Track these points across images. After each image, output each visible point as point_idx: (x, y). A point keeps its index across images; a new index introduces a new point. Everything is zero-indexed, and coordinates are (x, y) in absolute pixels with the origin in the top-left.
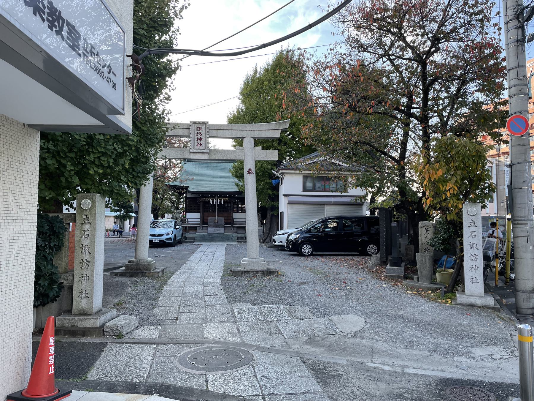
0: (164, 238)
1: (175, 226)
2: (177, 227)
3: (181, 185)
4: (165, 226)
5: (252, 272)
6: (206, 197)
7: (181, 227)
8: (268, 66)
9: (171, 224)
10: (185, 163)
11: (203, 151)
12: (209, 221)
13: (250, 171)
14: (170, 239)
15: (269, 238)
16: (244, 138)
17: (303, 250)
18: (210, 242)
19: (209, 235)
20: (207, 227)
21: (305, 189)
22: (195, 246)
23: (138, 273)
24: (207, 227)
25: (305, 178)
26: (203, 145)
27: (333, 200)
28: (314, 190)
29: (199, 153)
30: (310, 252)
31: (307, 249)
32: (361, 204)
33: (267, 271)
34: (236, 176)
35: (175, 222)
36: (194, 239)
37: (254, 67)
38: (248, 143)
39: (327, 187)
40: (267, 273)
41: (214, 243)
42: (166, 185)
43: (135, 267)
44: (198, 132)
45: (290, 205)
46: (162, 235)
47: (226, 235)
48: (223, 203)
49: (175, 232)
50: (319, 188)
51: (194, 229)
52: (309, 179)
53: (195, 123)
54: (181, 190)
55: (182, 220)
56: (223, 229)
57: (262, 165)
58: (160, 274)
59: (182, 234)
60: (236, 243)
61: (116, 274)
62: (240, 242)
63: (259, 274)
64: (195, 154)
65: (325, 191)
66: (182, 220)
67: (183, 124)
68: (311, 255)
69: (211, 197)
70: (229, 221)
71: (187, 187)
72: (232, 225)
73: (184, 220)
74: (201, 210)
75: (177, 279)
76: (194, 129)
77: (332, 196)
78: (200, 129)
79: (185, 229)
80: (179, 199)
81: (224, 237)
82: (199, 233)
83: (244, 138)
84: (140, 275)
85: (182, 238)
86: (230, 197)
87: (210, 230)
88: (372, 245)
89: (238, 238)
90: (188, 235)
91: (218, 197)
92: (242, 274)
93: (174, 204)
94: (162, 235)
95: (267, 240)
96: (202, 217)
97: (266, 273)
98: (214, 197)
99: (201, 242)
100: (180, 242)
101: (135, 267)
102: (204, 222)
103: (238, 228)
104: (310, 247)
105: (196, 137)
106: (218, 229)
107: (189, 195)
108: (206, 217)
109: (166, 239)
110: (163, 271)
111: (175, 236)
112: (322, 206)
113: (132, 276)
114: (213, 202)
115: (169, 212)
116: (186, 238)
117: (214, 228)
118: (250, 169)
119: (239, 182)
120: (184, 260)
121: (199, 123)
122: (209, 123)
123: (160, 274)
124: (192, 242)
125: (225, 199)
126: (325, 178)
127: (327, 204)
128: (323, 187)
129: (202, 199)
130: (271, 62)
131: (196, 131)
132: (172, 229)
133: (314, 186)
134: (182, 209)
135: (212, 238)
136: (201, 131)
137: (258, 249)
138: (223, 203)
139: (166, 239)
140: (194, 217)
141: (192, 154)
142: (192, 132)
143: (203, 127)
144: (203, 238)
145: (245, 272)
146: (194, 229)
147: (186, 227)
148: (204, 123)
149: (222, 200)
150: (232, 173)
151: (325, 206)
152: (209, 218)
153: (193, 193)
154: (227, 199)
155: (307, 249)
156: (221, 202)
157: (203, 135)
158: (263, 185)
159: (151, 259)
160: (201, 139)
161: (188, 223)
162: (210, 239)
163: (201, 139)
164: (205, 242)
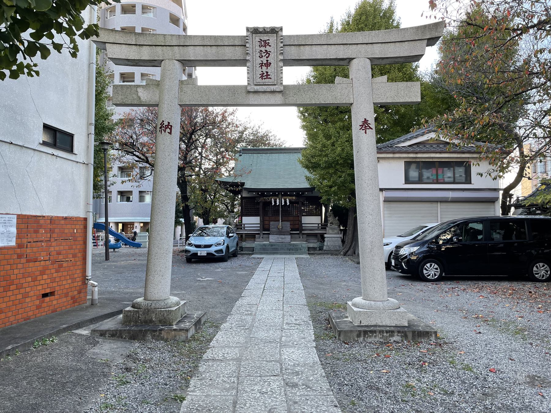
0: (212, 250)
1: (228, 233)
2: (230, 235)
3: (236, 181)
4: (215, 234)
5: (381, 332)
6: (266, 196)
7: (235, 235)
8: (348, 17)
9: (222, 231)
10: (240, 155)
11: (272, 88)
12: (271, 226)
13: (365, 125)
14: (221, 251)
15: (352, 250)
16: (351, 59)
17: (425, 272)
18: (274, 254)
19: (272, 245)
20: (269, 234)
21: (407, 181)
22: (254, 261)
23: (146, 331)
24: (269, 234)
25: (408, 164)
26: (272, 76)
27: (451, 195)
28: (420, 181)
29: (264, 92)
30: (438, 274)
31: (431, 270)
32: (493, 201)
33: (414, 332)
34: (307, 167)
35: (228, 228)
36: (252, 251)
37: (329, 22)
38: (360, 69)
39: (440, 177)
40: (413, 336)
41: (278, 256)
42: (217, 181)
43: (142, 317)
44: (263, 49)
45: (387, 204)
46: (209, 246)
47: (294, 245)
48: (288, 204)
49: (227, 241)
50: (428, 178)
51: (252, 237)
52: (413, 166)
53: (255, 31)
54: (235, 188)
55: (237, 225)
56: (289, 237)
57: (343, 150)
58: (192, 332)
59: (237, 244)
60: (308, 256)
61: (103, 334)
62: (313, 254)
63: (396, 338)
64: (256, 96)
65: (438, 183)
66: (237, 225)
67: (234, 37)
68: (440, 279)
69: (272, 196)
70: (297, 226)
71: (243, 184)
72: (301, 232)
73: (239, 226)
74: (261, 212)
75: (225, 343)
76: (254, 44)
77: (448, 189)
78: (266, 43)
79: (241, 237)
80: (234, 200)
81: (291, 247)
82: (258, 243)
83: (351, 59)
84: (149, 337)
85: (236, 249)
86: (297, 195)
87: (273, 238)
88: (541, 264)
89: (309, 249)
90: (245, 244)
91: (283, 196)
92: (359, 336)
93: (227, 207)
94: (209, 246)
95: (349, 252)
96: (262, 222)
97: (410, 335)
98: (277, 196)
99: (261, 253)
100: (234, 255)
101: (142, 317)
102: (265, 228)
103: (308, 235)
104: (436, 266)
105: (259, 61)
106: (283, 236)
107: (245, 194)
108: (267, 222)
109: (216, 251)
110: (198, 323)
111: (228, 247)
112: (434, 205)
113: (133, 337)
114: (275, 202)
115: (222, 216)
116: (242, 249)
117: (278, 236)
118: (366, 121)
119: (311, 175)
120: (238, 289)
121: (265, 31)
122: (285, 33)
123: (192, 332)
124: (250, 254)
125: (291, 198)
126: (437, 164)
127: (441, 202)
128: (435, 177)
129: (262, 198)
130: (353, 12)
131: (258, 48)
132: (223, 238)
133: (421, 175)
134: (237, 213)
135: (276, 249)
136: (268, 48)
137: (385, 281)
138: (288, 204)
139: (216, 251)
140: (252, 222)
141: (251, 95)
142: (250, 51)
143: (272, 39)
144: (264, 249)
145: (366, 332)
146: (252, 237)
147: (241, 235)
148: (274, 31)
149: (288, 201)
150: (302, 163)
151: (439, 204)
152: (271, 223)
153: (250, 190)
154: (294, 198)
155: (431, 270)
156: (285, 202)
157: (272, 55)
158: (345, 177)
159: (175, 299)
160: (268, 64)
161: (246, 230)
162: (273, 250)
163: (268, 64)
164: (267, 254)
